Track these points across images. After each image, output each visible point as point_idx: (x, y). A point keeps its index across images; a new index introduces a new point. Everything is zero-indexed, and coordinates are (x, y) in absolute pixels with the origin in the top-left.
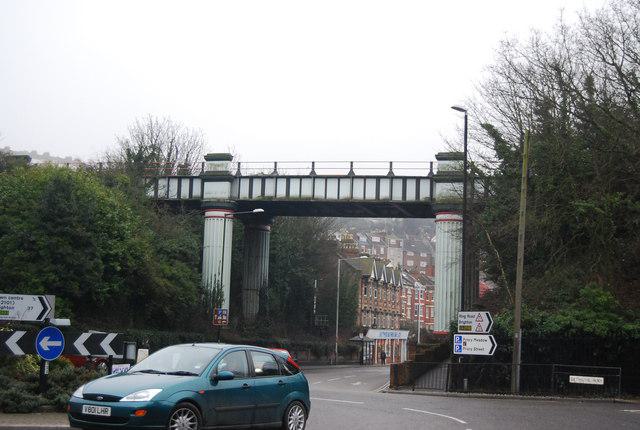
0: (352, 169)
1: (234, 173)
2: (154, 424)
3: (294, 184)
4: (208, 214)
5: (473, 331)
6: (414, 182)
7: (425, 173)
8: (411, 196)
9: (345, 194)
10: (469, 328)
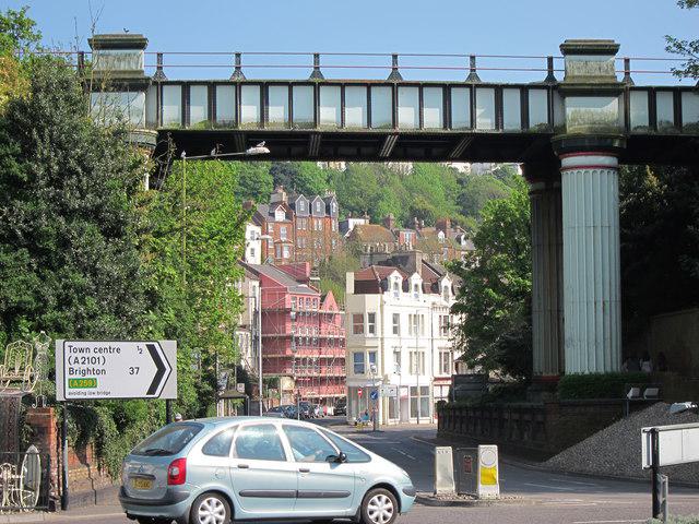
2: (612, 518)
4: (567, 161)
6: (517, 94)
8: (512, 123)
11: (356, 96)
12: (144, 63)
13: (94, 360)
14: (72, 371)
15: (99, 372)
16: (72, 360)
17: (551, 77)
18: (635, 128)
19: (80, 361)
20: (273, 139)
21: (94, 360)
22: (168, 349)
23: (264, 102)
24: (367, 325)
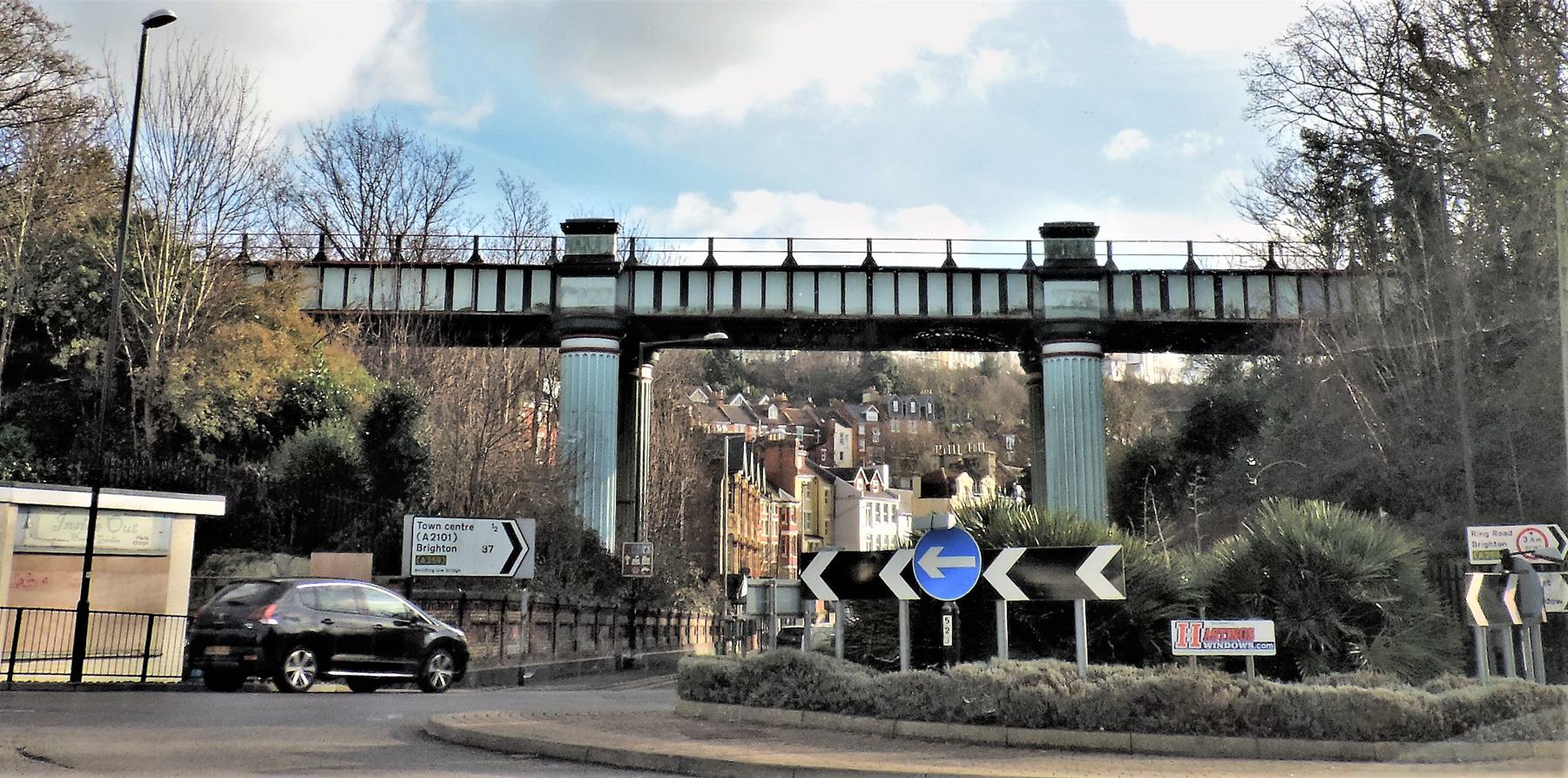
0: (869, 254)
4: (1048, 348)
7: (1018, 263)
9: (856, 306)
11: (830, 285)
15: (449, 549)
17: (1029, 262)
20: (724, 323)
23: (1218, 288)
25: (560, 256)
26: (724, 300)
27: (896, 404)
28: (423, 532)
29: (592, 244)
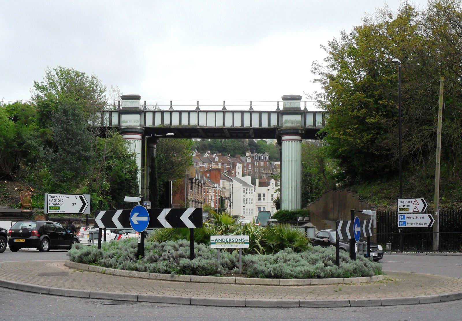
1: (302, 108)
3: (185, 116)
4: (284, 138)
5: (411, 211)
7: (274, 109)
10: (408, 209)
11: (211, 116)
12: (140, 104)
13: (59, 201)
14: (50, 204)
15: (60, 204)
16: (51, 200)
17: (278, 108)
18: (308, 126)
19: (54, 201)
21: (59, 201)
22: (87, 198)
24: (262, 197)
25: (281, 108)
26: (175, 122)
27: (262, 157)
28: (51, 199)
29: (293, 104)
